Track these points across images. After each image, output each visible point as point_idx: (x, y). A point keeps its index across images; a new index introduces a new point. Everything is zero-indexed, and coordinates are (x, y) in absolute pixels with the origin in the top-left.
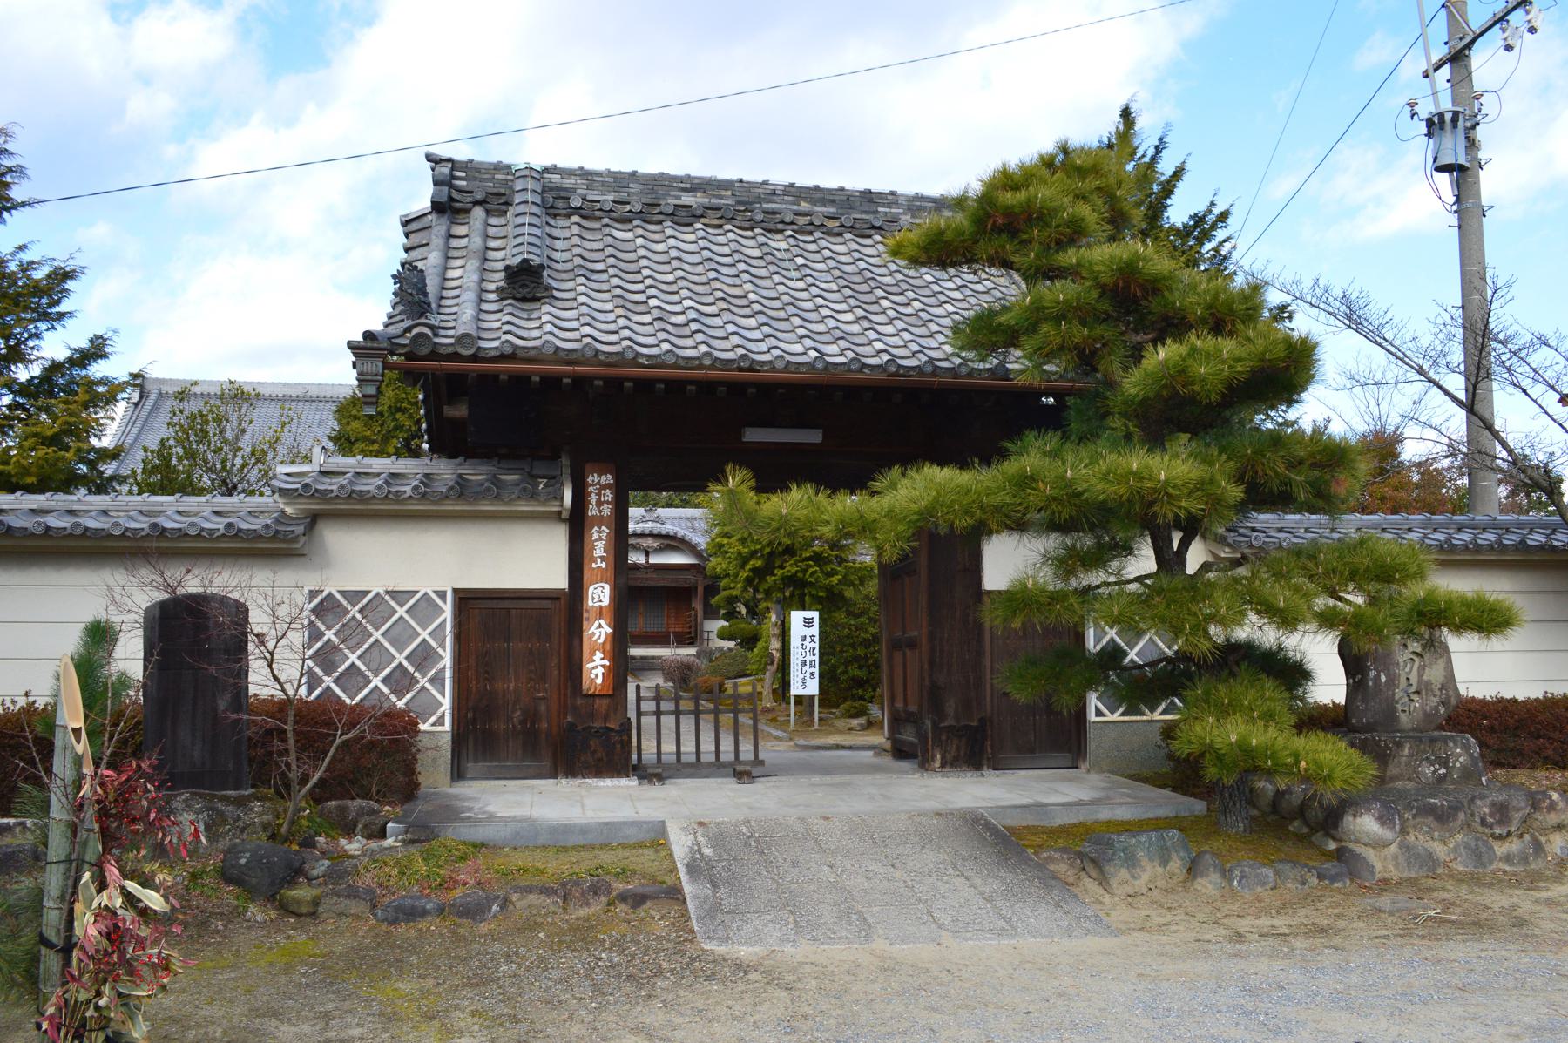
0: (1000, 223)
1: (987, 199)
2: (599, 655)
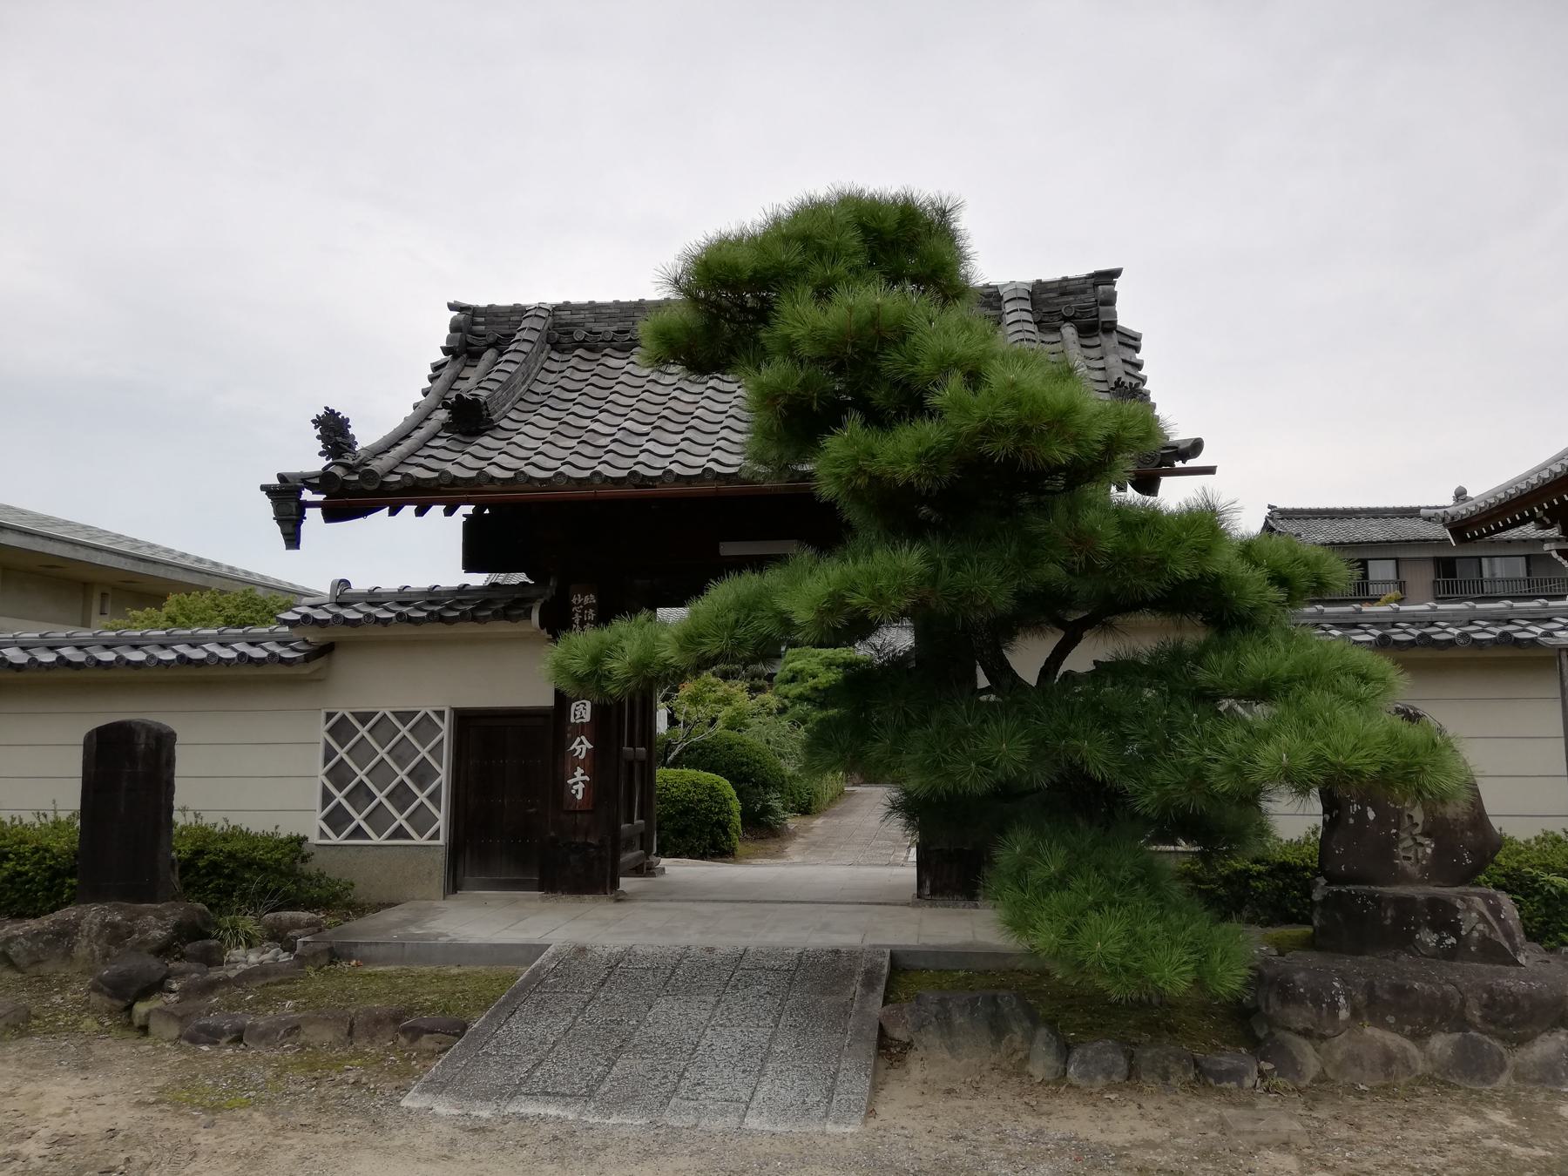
0: (730, 305)
1: (1060, 282)
2: (580, 771)
